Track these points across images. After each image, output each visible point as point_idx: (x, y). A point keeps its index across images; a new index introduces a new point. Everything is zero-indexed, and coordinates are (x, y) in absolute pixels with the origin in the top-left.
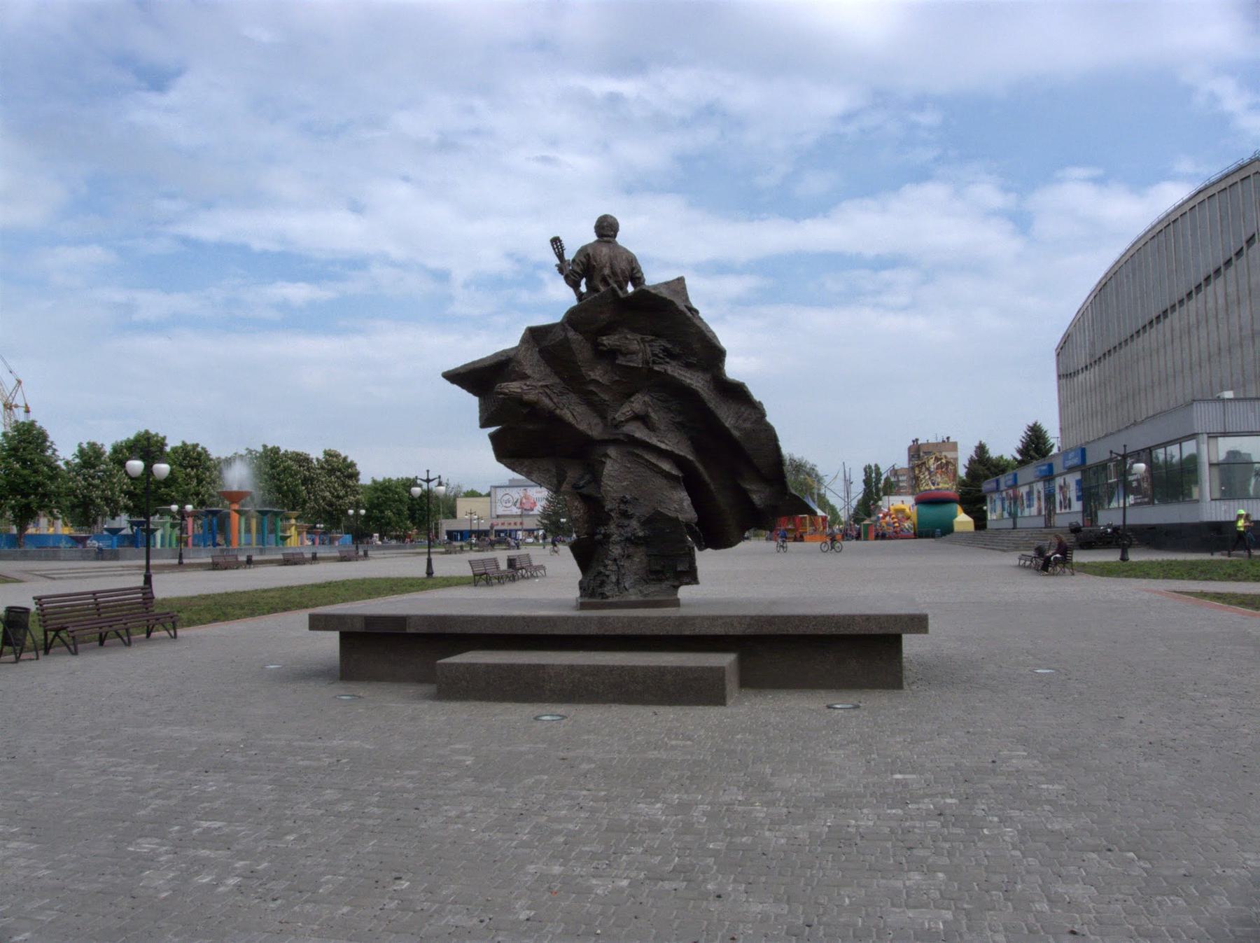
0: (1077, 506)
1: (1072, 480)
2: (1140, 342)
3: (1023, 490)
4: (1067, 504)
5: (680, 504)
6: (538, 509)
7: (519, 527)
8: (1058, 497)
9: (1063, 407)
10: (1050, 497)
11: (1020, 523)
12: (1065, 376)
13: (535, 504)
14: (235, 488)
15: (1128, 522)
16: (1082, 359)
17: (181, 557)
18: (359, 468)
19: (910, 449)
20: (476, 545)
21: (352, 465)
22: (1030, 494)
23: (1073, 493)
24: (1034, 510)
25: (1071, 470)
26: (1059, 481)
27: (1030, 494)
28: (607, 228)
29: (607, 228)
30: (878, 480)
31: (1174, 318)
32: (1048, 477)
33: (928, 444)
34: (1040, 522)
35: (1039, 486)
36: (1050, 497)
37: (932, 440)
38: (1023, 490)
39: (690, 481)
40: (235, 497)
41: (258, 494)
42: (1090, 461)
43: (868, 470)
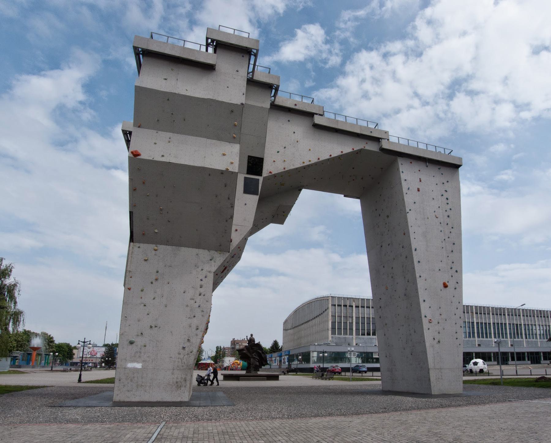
0: (287, 363)
1: (286, 357)
2: (303, 326)
3: (274, 359)
4: (284, 363)
5: (258, 363)
6: (99, 355)
7: (91, 361)
8: (283, 361)
9: (284, 337)
10: (280, 361)
11: (272, 367)
12: (285, 330)
13: (97, 354)
14: (36, 346)
15: (250, 37)
16: (289, 326)
17: (52, 368)
18: (54, 339)
19: (231, 342)
20: (104, 367)
21: (52, 338)
22: (275, 360)
23: (286, 360)
24: (276, 364)
25: (286, 355)
26: (283, 357)
27: (275, 360)
28: (252, 335)
29: (252, 335)
30: (220, 351)
31: (310, 323)
32: (281, 356)
33: (238, 340)
34: (278, 367)
35: (278, 358)
36: (280, 361)
37: (239, 339)
38: (274, 359)
39: (259, 362)
40: (35, 349)
41: (43, 348)
42: (291, 353)
43: (217, 348)
